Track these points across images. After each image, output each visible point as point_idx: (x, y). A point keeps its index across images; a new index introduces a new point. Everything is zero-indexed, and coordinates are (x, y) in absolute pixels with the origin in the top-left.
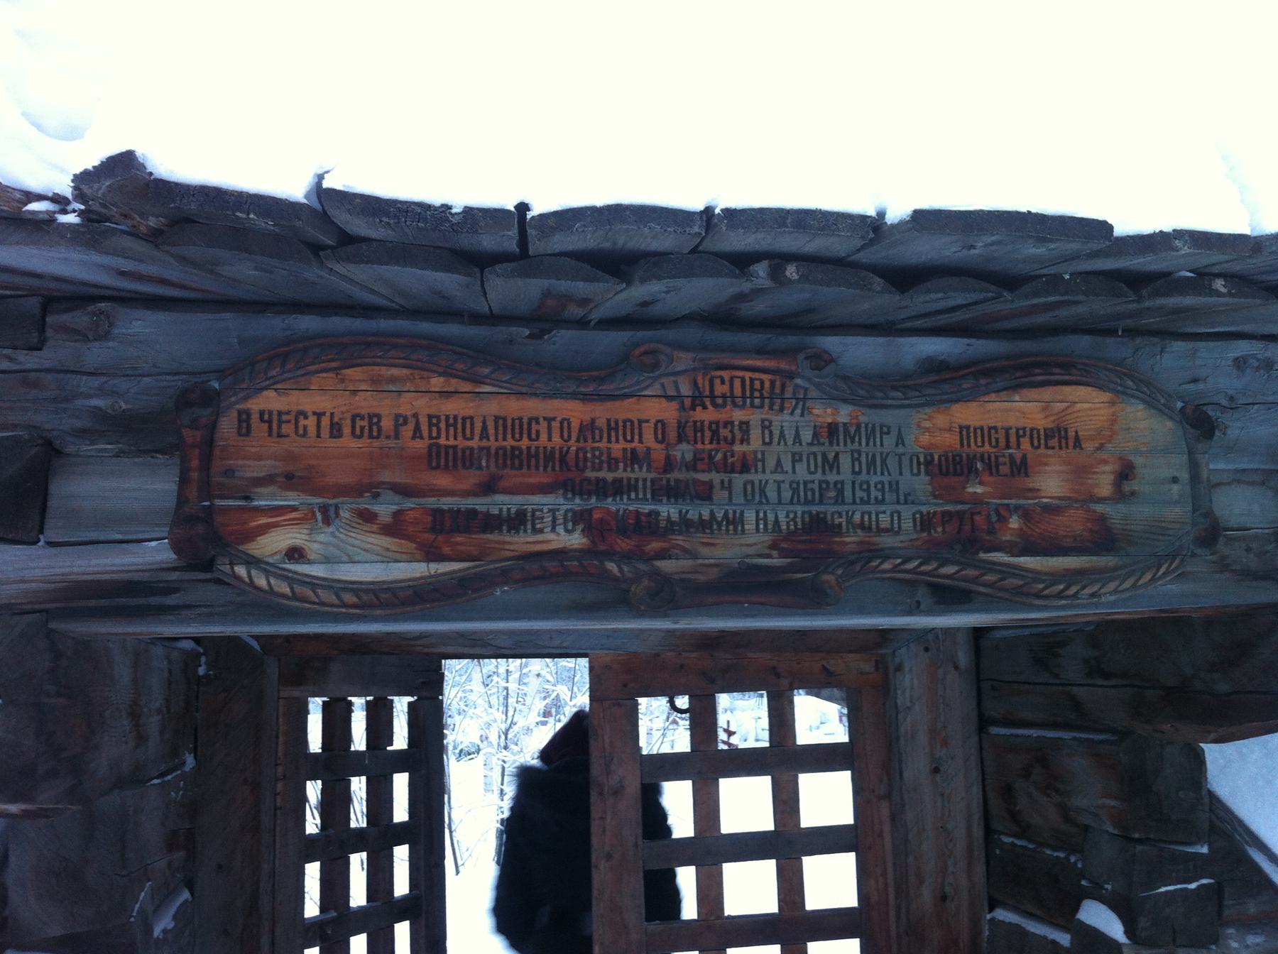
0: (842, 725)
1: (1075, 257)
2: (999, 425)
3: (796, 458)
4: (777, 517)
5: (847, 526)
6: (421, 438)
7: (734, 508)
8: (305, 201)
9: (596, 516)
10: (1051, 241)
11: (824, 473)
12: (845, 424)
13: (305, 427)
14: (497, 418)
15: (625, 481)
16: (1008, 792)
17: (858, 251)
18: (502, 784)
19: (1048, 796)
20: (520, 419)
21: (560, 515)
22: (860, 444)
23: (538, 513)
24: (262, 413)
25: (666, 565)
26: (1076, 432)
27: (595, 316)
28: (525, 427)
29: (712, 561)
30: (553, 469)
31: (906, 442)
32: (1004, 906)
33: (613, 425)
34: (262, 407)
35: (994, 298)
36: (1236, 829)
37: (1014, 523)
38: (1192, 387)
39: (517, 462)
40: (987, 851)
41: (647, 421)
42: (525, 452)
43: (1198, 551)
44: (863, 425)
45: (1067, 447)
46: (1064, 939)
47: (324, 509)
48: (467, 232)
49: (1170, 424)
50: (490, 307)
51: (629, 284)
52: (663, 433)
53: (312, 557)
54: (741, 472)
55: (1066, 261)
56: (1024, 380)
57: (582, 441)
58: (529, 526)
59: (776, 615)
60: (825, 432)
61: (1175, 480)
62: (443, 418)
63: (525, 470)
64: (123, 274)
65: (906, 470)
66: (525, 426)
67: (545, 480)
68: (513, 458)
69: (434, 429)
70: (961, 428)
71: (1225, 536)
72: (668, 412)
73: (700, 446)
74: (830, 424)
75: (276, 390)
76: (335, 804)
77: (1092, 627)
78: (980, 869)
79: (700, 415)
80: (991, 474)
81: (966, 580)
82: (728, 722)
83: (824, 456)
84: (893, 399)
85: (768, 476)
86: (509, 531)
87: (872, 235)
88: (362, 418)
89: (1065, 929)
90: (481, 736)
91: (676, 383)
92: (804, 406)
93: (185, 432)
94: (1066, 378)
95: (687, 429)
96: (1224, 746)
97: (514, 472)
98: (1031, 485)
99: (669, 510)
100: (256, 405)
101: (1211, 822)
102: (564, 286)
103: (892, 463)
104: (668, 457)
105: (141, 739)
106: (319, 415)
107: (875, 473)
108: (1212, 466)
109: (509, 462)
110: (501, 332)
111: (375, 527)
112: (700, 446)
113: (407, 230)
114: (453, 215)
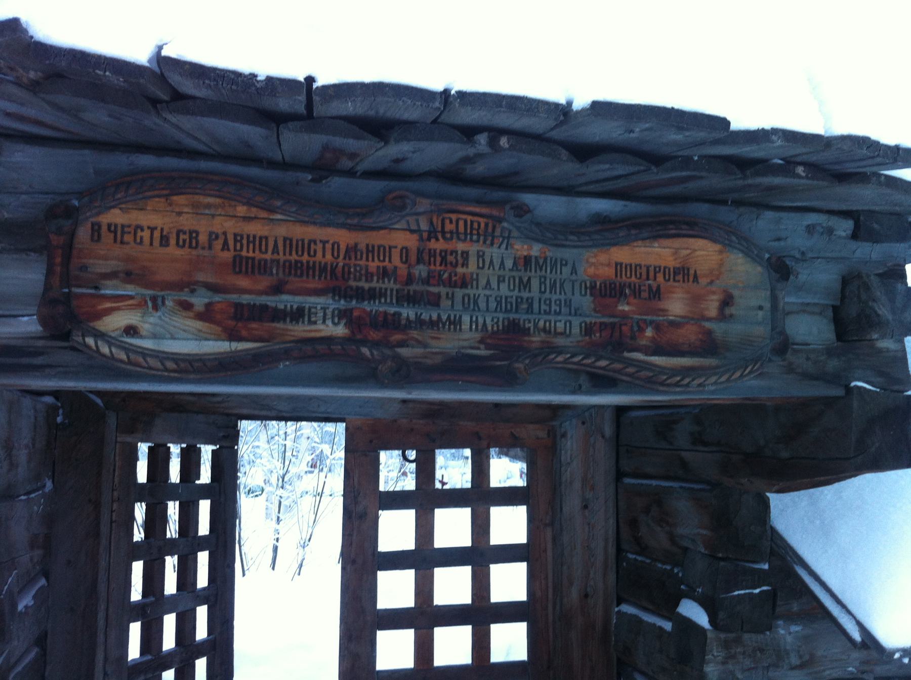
0: (521, 480)
1: (702, 143)
2: (643, 263)
3: (501, 280)
4: (485, 321)
5: (534, 329)
6: (228, 250)
7: (455, 313)
8: (147, 64)
9: (356, 314)
10: (687, 130)
11: (520, 291)
12: (536, 257)
13: (141, 238)
14: (285, 239)
15: (378, 290)
16: (634, 523)
17: (552, 129)
18: (279, 512)
19: (662, 527)
20: (303, 241)
21: (329, 312)
22: (546, 271)
23: (313, 310)
24: (109, 225)
25: (404, 352)
26: (695, 271)
27: (361, 168)
28: (306, 246)
29: (438, 350)
30: (326, 278)
31: (578, 273)
32: (627, 602)
33: (370, 248)
34: (109, 221)
35: (645, 171)
36: (788, 553)
37: (649, 332)
38: (776, 244)
39: (299, 272)
40: (617, 563)
41: (396, 247)
42: (305, 264)
43: (774, 358)
44: (549, 259)
45: (688, 281)
46: (668, 626)
47: (154, 299)
48: (268, 95)
49: (759, 269)
50: (283, 156)
51: (387, 143)
52: (407, 256)
53: (144, 333)
54: (461, 287)
55: (696, 145)
56: (661, 233)
57: (347, 258)
58: (306, 319)
59: (480, 390)
60: (522, 262)
61: (761, 308)
62: (245, 237)
63: (305, 278)
64: (8, 115)
65: (577, 291)
66: (306, 246)
67: (320, 286)
68: (296, 268)
69: (238, 245)
70: (616, 264)
71: (793, 349)
72: (411, 241)
73: (432, 267)
74: (525, 257)
75: (120, 209)
76: (156, 520)
77: (697, 411)
78: (612, 577)
79: (433, 245)
80: (635, 297)
81: (614, 371)
82: (443, 476)
83: (521, 279)
84: (571, 240)
85: (480, 291)
86: (291, 321)
87: (562, 118)
88: (185, 233)
89: (669, 619)
90: (265, 480)
91: (417, 221)
92: (508, 242)
93: (52, 237)
94: (691, 232)
95: (424, 254)
96: (785, 495)
97: (297, 279)
98: (662, 307)
99: (408, 312)
100: (106, 219)
101: (771, 547)
102: (338, 141)
103: (568, 287)
104: (409, 274)
105: (13, 466)
106: (152, 229)
107: (555, 293)
108: (786, 300)
109: (293, 272)
110: (290, 176)
111: (191, 314)
112: (432, 267)
113: (223, 91)
114: (258, 82)
